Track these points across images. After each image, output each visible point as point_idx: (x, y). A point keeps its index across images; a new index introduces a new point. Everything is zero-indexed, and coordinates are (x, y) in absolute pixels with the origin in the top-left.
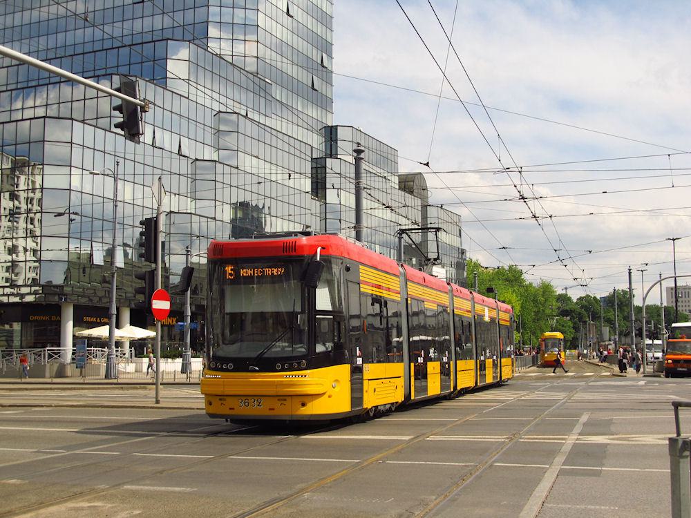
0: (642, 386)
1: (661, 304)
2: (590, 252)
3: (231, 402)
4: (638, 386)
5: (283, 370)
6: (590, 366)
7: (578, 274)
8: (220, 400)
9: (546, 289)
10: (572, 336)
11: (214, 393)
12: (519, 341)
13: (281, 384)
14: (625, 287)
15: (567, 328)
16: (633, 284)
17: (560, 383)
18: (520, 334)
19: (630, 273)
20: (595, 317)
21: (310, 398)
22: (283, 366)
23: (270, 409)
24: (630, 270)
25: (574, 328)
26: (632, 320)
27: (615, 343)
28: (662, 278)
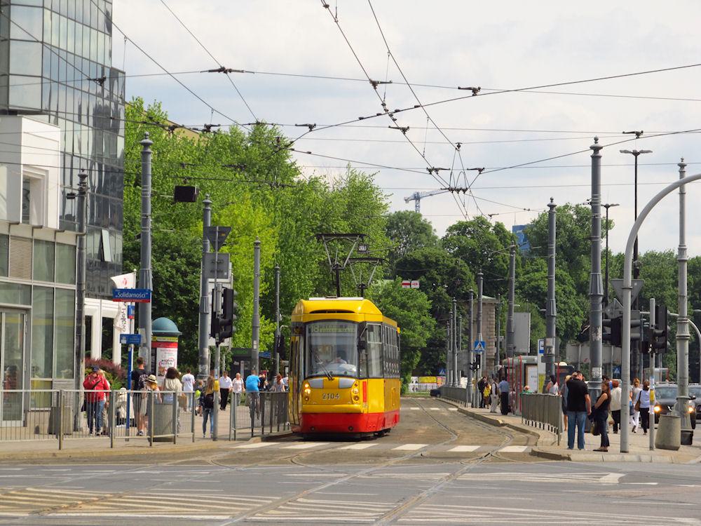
0: (609, 487)
1: (682, 250)
2: (475, 91)
4: (600, 487)
6: (474, 426)
9: (359, 196)
10: (428, 335)
14: (579, 196)
15: (415, 313)
16: (603, 190)
17: (379, 472)
19: (596, 159)
20: (495, 282)
24: (596, 149)
25: (433, 312)
26: (595, 296)
27: (547, 359)
28: (687, 175)
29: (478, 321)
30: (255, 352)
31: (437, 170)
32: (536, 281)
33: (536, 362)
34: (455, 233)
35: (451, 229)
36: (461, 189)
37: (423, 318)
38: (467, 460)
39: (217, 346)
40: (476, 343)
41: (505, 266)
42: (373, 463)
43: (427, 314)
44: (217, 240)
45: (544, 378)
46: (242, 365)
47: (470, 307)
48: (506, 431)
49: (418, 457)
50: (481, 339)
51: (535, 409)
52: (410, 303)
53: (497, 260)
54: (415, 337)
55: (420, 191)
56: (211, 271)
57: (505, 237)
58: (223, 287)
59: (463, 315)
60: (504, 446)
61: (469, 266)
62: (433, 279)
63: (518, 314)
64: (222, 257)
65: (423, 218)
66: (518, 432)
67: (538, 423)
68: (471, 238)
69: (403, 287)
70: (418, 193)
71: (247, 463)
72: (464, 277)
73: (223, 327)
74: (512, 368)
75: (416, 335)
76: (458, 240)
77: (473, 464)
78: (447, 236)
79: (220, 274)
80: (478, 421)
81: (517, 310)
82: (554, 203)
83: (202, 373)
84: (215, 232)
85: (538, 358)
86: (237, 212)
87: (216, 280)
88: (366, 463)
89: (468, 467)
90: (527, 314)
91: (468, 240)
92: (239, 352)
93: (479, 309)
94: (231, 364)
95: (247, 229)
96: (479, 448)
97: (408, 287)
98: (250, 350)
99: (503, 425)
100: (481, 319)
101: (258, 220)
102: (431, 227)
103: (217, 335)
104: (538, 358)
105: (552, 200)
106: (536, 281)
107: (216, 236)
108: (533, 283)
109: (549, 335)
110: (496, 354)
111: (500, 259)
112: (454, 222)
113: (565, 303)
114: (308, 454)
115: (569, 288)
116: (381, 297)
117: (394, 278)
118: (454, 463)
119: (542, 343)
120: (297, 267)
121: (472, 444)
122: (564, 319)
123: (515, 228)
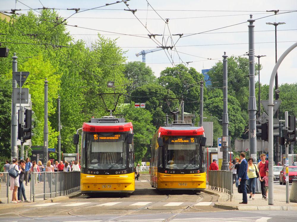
3: (98, 186)
5: (118, 174)
7: (157, 27)
8: (94, 185)
9: (108, 53)
11: (92, 183)
12: (57, 146)
13: (192, 178)
14: (239, 51)
15: (143, 124)
18: (58, 133)
19: (251, 27)
21: (128, 184)
22: (93, 172)
23: (114, 188)
24: (251, 22)
27: (224, 149)
30: (46, 148)
31: (154, 36)
32: (216, 103)
33: (216, 151)
34: (166, 74)
35: (163, 73)
37: (148, 126)
39: (22, 145)
41: (197, 94)
53: (192, 90)
58: (25, 109)
62: (154, 103)
64: (24, 91)
65: (147, 66)
69: (136, 107)
70: (144, 51)
71: (40, 215)
73: (25, 133)
79: (23, 101)
85: (218, 149)
86: (34, 64)
87: (20, 105)
88: (114, 214)
91: (174, 79)
92: (36, 149)
95: (40, 75)
97: (139, 107)
98: (43, 147)
102: (151, 71)
103: (22, 138)
104: (218, 149)
105: (225, 53)
106: (216, 103)
107: (20, 78)
108: (215, 104)
109: (224, 135)
113: (234, 116)
114: (78, 209)
115: (236, 107)
117: (130, 102)
119: (220, 140)
120: (71, 96)
121: (179, 201)
122: (234, 125)
123: (203, 71)
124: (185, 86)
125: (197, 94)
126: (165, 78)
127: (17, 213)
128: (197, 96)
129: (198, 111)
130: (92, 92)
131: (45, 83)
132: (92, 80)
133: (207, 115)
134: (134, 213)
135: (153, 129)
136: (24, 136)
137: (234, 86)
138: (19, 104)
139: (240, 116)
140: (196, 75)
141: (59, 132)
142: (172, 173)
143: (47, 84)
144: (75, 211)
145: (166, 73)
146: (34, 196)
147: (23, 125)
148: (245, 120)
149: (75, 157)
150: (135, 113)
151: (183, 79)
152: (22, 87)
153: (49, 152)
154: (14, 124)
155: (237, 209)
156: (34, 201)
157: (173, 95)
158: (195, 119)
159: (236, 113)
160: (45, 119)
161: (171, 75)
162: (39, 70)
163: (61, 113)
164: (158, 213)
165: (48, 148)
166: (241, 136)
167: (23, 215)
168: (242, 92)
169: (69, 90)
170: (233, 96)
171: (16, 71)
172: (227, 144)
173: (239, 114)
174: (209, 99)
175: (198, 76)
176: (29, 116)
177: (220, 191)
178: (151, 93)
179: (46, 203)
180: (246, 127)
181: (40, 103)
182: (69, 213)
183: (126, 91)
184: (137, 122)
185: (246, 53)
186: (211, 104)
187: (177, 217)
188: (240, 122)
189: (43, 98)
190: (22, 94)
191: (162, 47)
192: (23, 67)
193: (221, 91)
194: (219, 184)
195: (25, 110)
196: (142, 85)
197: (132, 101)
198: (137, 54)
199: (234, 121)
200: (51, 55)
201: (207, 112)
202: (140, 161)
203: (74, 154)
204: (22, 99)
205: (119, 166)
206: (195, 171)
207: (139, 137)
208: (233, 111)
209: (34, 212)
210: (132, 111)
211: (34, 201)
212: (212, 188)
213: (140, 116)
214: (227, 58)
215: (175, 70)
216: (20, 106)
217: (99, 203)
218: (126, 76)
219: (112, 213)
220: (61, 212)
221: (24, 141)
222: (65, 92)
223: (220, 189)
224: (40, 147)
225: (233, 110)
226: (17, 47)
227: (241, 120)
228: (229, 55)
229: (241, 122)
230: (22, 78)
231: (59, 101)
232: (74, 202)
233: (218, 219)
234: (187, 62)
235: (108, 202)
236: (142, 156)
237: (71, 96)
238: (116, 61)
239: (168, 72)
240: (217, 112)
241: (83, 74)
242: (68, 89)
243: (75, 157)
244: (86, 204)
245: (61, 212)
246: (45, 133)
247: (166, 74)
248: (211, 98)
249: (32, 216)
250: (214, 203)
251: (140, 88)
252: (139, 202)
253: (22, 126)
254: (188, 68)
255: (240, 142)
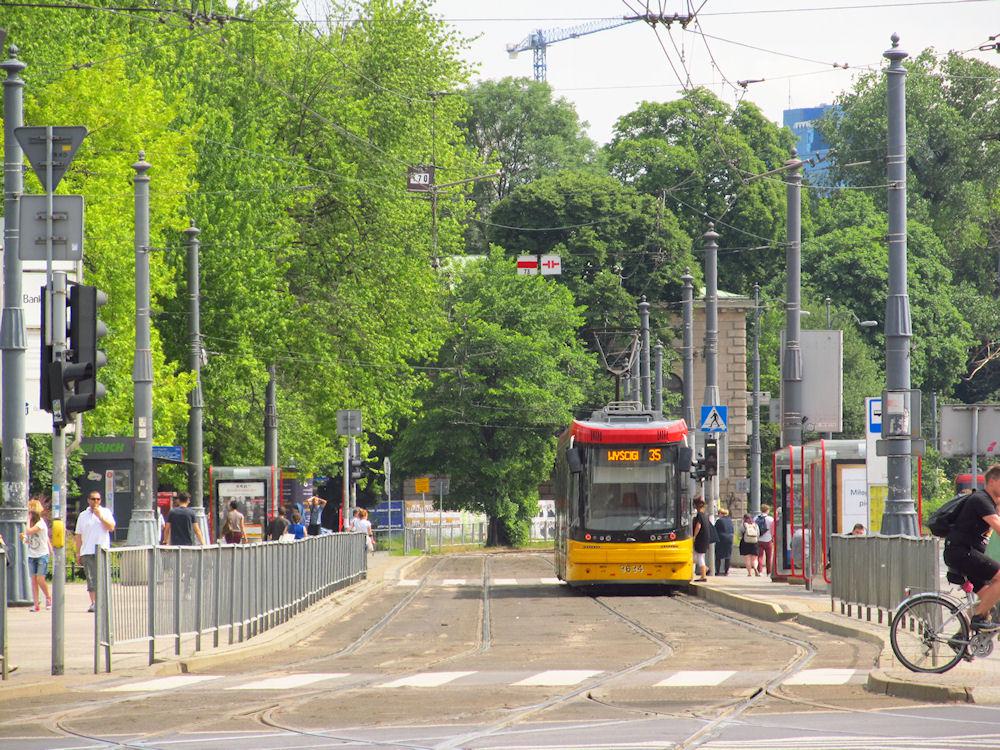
15: (542, 339)
20: (746, 255)
27: (891, 446)
29: (708, 356)
30: (144, 446)
32: (848, 249)
33: (861, 456)
34: (637, 131)
35: (625, 124)
36: (676, 17)
37: (565, 352)
38: (709, 708)
39: (58, 433)
40: (705, 411)
41: (769, 215)
42: (471, 720)
43: (573, 341)
44: (50, 161)
45: (885, 494)
46: (109, 481)
47: (686, 319)
48: (794, 633)
49: (582, 704)
50: (717, 401)
51: (846, 569)
52: (528, 314)
53: (746, 197)
54: (544, 400)
55: (544, 26)
56: (37, 242)
57: (766, 137)
58: (68, 282)
59: (665, 340)
60: (796, 670)
61: (676, 213)
62: (584, 250)
63: (811, 333)
64: (63, 206)
65: (555, 97)
66: (827, 635)
67: (874, 611)
68: (679, 143)
69: (521, 271)
70: (540, 33)
71: (148, 729)
72: (667, 244)
73: (71, 384)
74: (800, 472)
75: (548, 395)
76: (646, 149)
77: (725, 719)
78: (616, 141)
79: (61, 248)
80: (720, 609)
81: (811, 324)
82: (901, 48)
83: (10, 503)
84: (44, 142)
85: (868, 444)
86: (86, 91)
87: (49, 265)
88: (454, 721)
89: (712, 723)
90: (832, 333)
91: (671, 151)
92: (101, 449)
93: (710, 325)
94: (81, 481)
95: (116, 136)
96: (733, 678)
97: (534, 271)
98: (132, 443)
99: (785, 616)
100: (715, 349)
101: (140, 111)
102: (575, 116)
103: (56, 404)
104: (868, 444)
105: (895, 40)
106: (848, 249)
107: (45, 150)
108: (841, 256)
109: (895, 386)
110: (751, 439)
111: (755, 196)
112: (631, 107)
114: (302, 702)
115: (932, 266)
116: (453, 299)
117: (487, 250)
118: (677, 715)
119: (877, 406)
120: (242, 227)
121: (714, 667)
122: (923, 344)
123: (789, 115)
124: (716, 180)
125: (769, 215)
126: (634, 148)
127: (51, 719)
128: (767, 221)
129: (770, 287)
130: (328, 208)
131: (133, 171)
132: (328, 155)
133: (810, 302)
134: (540, 716)
135: (585, 363)
136: (66, 399)
137: (922, 179)
138: (45, 262)
139: (949, 304)
140: (762, 134)
141: (196, 373)
142: (605, 541)
143: (145, 177)
144: (290, 710)
145: (637, 124)
146: (108, 648)
147: (63, 349)
148: (968, 321)
149: (265, 481)
150: (507, 296)
151: (708, 150)
152: (54, 190)
153: (158, 461)
154: (15, 347)
155: (968, 699)
156: (109, 670)
157: (669, 217)
158: (761, 320)
159: (931, 291)
160: (138, 323)
161: (657, 134)
162: (106, 115)
163: (202, 300)
164: (638, 716)
165: (153, 443)
166: (953, 391)
167: (73, 729)
168: (957, 203)
169: (235, 200)
170: (921, 221)
171: (21, 123)
172: (906, 426)
173: (943, 297)
174: (818, 234)
175: (773, 136)
176: (84, 312)
177: (880, 621)
178: (575, 214)
179: (159, 675)
180: (972, 350)
181: (113, 256)
182: (266, 718)
183: (472, 204)
184: (519, 336)
185: (992, 38)
186: (826, 256)
187: (721, 735)
188: (951, 328)
189: (129, 235)
190: (54, 220)
191: (645, 18)
192: (43, 104)
193: (867, 202)
194: (878, 593)
195: (69, 286)
196: (538, 177)
197: (492, 245)
198: (512, 47)
199: (921, 324)
200: (157, 56)
201: (809, 288)
202: (534, 495)
203: (261, 471)
204: (54, 242)
205: (658, 523)
206: (663, 535)
207: (528, 397)
208: (921, 282)
209: (117, 715)
210: (493, 289)
211: (109, 670)
212: (846, 610)
213: (529, 309)
214: (904, 60)
215: (672, 113)
216: (49, 271)
217: (381, 676)
218: (472, 141)
219: (446, 718)
220: (230, 714)
221: (67, 416)
222: (217, 209)
223: (880, 612)
224: (121, 437)
225: (917, 281)
226: (19, 19)
227: (952, 320)
228: (911, 49)
229: (952, 331)
230: (54, 154)
231: (197, 248)
232: (278, 673)
233: (896, 743)
234: (742, 79)
235: (419, 671)
236: (540, 475)
237: (242, 227)
238: (431, 80)
239: (647, 123)
240: (853, 286)
241: (290, 135)
242: (230, 197)
243: (265, 481)
244: (331, 680)
245: (230, 714)
246: (141, 383)
247: (637, 131)
248: (825, 230)
249: (111, 732)
250: (867, 672)
251: (531, 191)
252: (549, 673)
253: (58, 354)
254: (727, 105)
255: (961, 414)
